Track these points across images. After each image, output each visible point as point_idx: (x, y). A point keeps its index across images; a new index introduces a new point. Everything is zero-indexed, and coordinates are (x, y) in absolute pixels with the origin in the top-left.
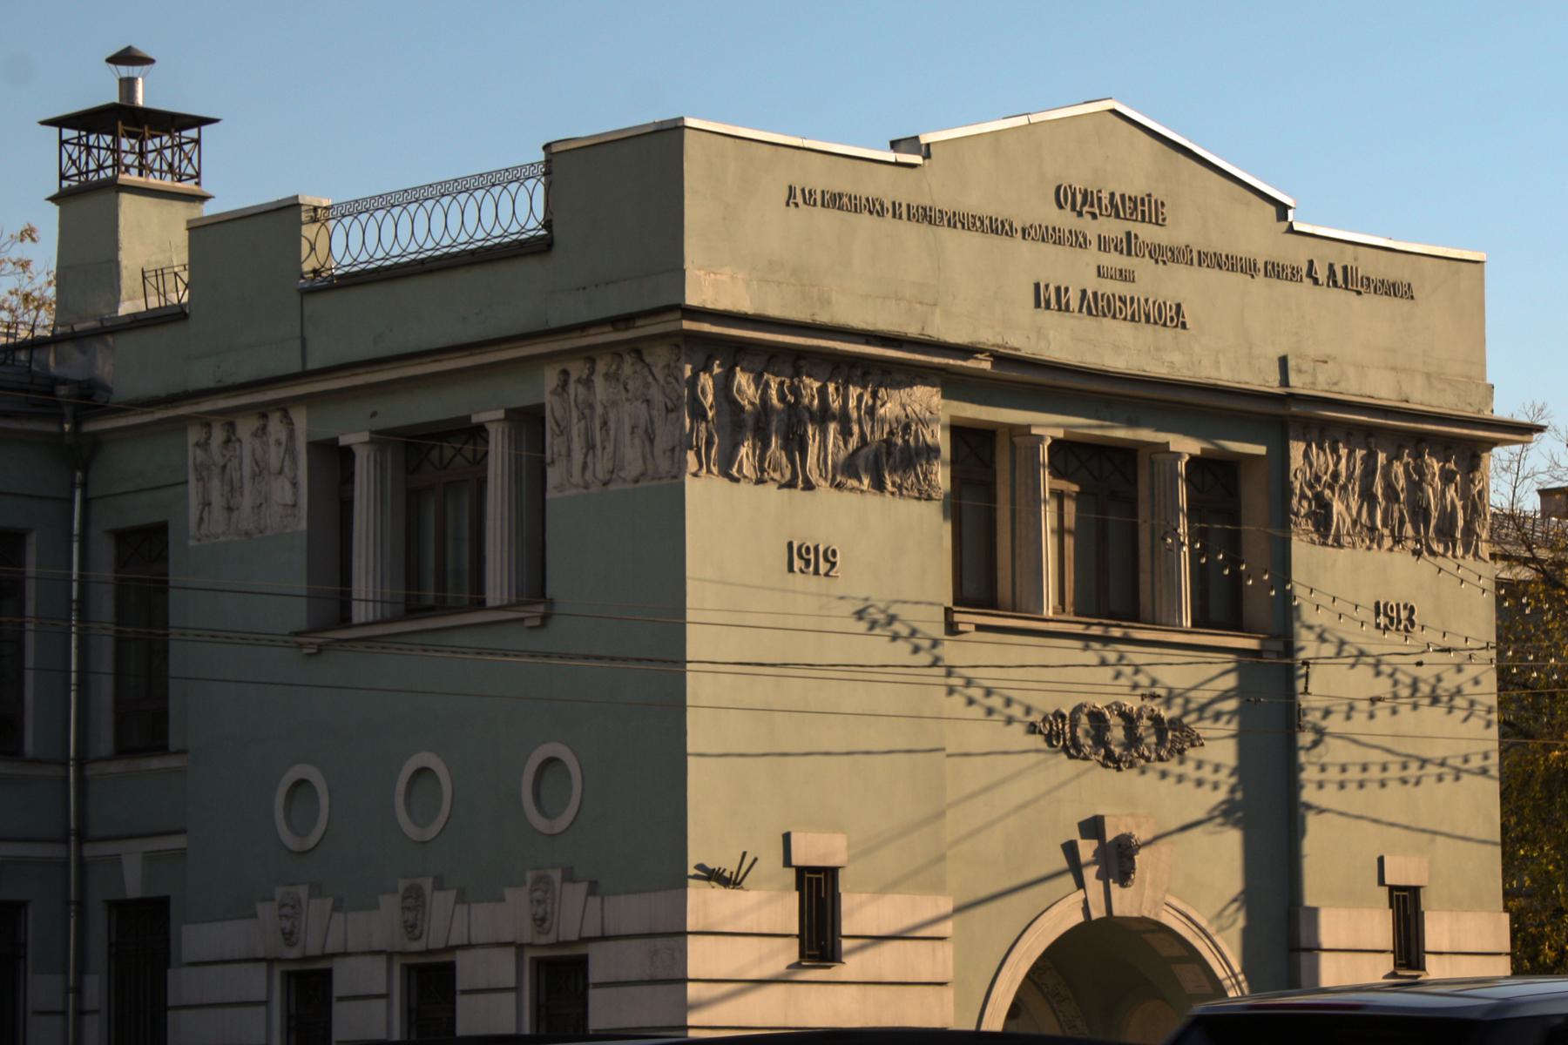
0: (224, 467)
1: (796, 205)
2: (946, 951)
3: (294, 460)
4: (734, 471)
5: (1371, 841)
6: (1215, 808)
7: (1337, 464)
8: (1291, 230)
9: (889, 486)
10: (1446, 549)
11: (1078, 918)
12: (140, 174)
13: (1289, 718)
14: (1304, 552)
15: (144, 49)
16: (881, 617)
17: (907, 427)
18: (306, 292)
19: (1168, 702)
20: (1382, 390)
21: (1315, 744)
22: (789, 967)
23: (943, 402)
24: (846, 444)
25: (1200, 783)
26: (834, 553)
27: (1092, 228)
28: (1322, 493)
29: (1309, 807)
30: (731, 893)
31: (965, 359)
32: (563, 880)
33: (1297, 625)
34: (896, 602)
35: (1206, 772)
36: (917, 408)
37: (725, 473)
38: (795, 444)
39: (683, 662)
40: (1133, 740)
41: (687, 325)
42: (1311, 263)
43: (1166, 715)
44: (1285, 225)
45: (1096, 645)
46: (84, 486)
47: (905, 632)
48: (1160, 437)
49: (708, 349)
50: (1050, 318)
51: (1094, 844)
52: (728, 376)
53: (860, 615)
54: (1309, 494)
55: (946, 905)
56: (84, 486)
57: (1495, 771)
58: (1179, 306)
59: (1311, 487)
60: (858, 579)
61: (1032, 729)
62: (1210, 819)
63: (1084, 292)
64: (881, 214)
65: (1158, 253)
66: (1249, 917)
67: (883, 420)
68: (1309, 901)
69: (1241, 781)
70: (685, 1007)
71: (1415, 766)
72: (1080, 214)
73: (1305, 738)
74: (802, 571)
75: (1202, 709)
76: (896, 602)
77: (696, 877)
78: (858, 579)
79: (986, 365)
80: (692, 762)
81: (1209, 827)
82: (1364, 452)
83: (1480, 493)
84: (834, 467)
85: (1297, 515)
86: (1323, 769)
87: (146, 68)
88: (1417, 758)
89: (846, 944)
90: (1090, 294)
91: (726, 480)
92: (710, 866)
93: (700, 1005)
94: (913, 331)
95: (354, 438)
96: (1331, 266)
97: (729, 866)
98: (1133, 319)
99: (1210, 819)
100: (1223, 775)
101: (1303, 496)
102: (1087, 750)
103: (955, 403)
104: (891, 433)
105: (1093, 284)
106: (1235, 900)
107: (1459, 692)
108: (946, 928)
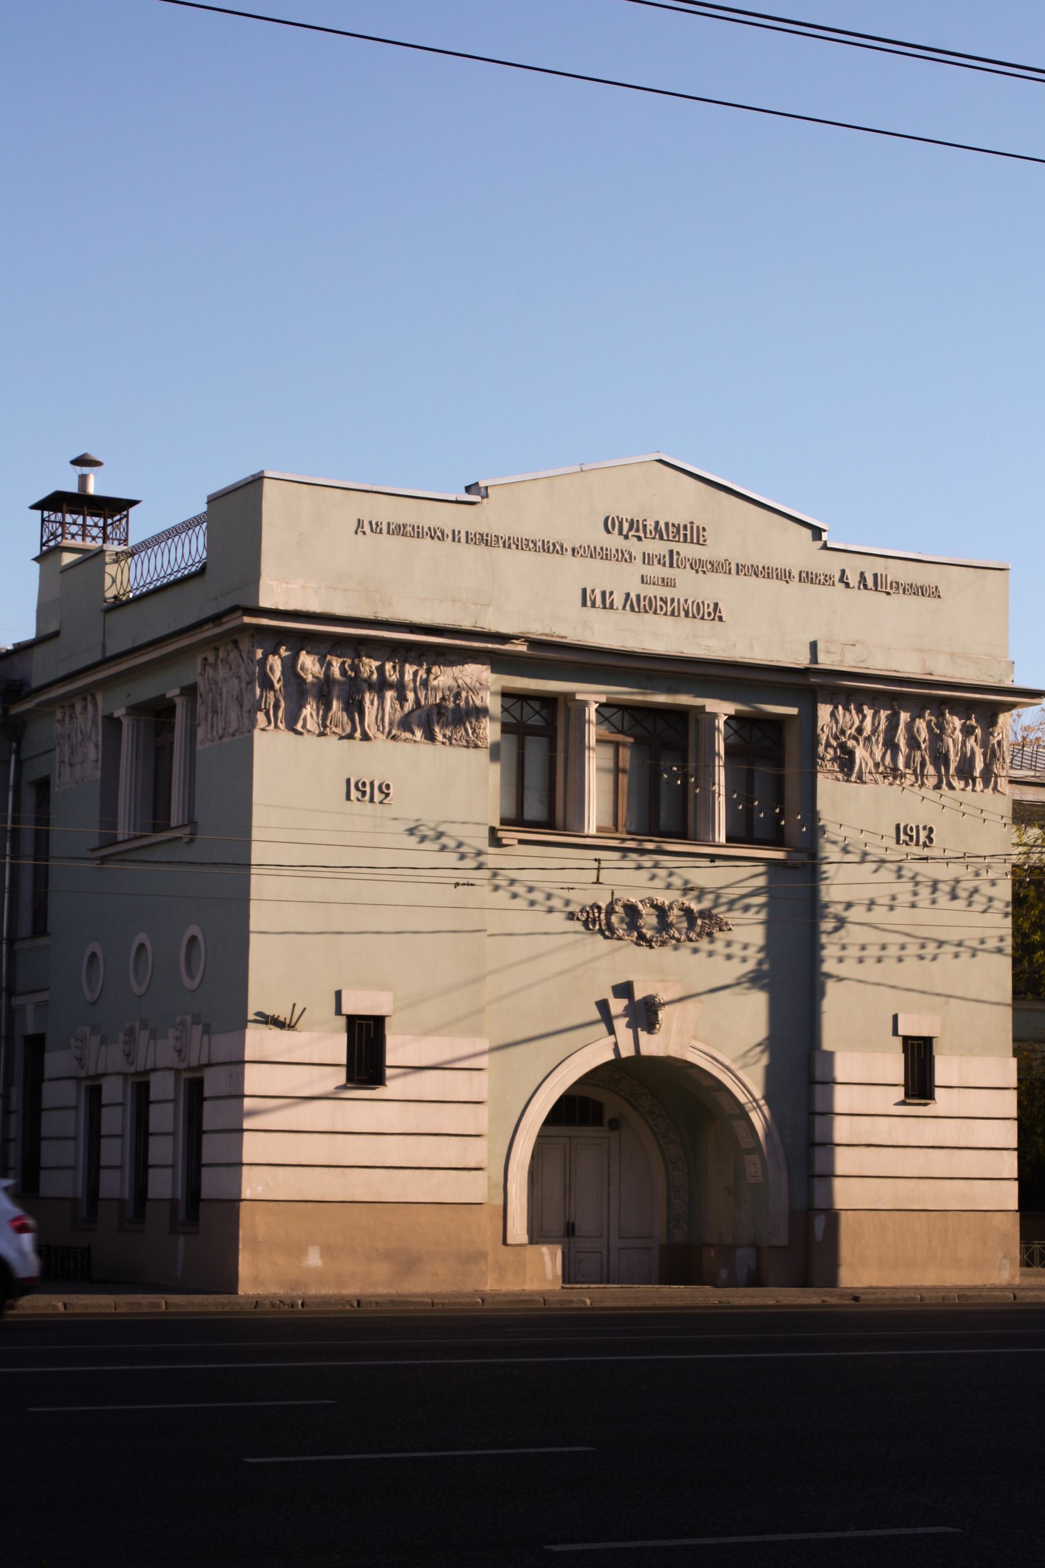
0: (69, 736)
1: (364, 533)
2: (483, 1076)
3: (97, 727)
4: (299, 727)
5: (889, 1002)
6: (743, 976)
7: (862, 722)
8: (825, 547)
9: (440, 737)
10: (967, 785)
11: (610, 1056)
12: (83, 540)
13: (812, 909)
14: (828, 788)
15: (96, 456)
16: (431, 833)
17: (457, 695)
18: (108, 611)
19: (699, 899)
20: (909, 666)
21: (836, 929)
22: (337, 1088)
23: (495, 676)
24: (402, 707)
25: (729, 957)
26: (388, 787)
27: (636, 548)
28: (845, 742)
29: (829, 976)
30: (285, 1034)
31: (504, 644)
32: (193, 1023)
33: (822, 841)
34: (445, 822)
35: (736, 950)
36: (468, 681)
37: (291, 727)
38: (354, 707)
39: (249, 865)
40: (664, 924)
41: (247, 620)
42: (843, 572)
43: (695, 907)
44: (820, 544)
45: (634, 856)
46: (18, 752)
47: (452, 844)
48: (699, 701)
49: (275, 638)
50: (590, 613)
51: (625, 1002)
52: (295, 657)
53: (411, 832)
54: (834, 744)
55: (484, 1044)
56: (18, 752)
57: (1009, 950)
58: (716, 605)
59: (836, 738)
60: (409, 803)
61: (571, 916)
62: (738, 984)
63: (628, 595)
64: (441, 539)
65: (697, 566)
66: (773, 1058)
67: (435, 689)
68: (827, 1045)
69: (767, 956)
70: (242, 1114)
71: (931, 946)
72: (626, 537)
73: (827, 925)
74: (358, 800)
75: (732, 903)
76: (445, 822)
77: (255, 1021)
78: (409, 803)
79: (523, 648)
80: (253, 939)
81: (737, 989)
82: (889, 712)
83: (999, 743)
84: (391, 724)
85: (823, 759)
86: (844, 947)
87: (95, 469)
88: (934, 940)
89: (389, 1072)
90: (633, 596)
91: (292, 734)
92: (267, 1013)
93: (253, 1113)
94: (467, 624)
95: (120, 713)
96: (862, 574)
97: (284, 1014)
98: (673, 614)
99: (738, 984)
100: (751, 952)
101: (828, 745)
102: (621, 932)
103: (506, 677)
104: (443, 699)
105: (636, 588)
106: (760, 1044)
107: (976, 891)
108: (483, 1062)
